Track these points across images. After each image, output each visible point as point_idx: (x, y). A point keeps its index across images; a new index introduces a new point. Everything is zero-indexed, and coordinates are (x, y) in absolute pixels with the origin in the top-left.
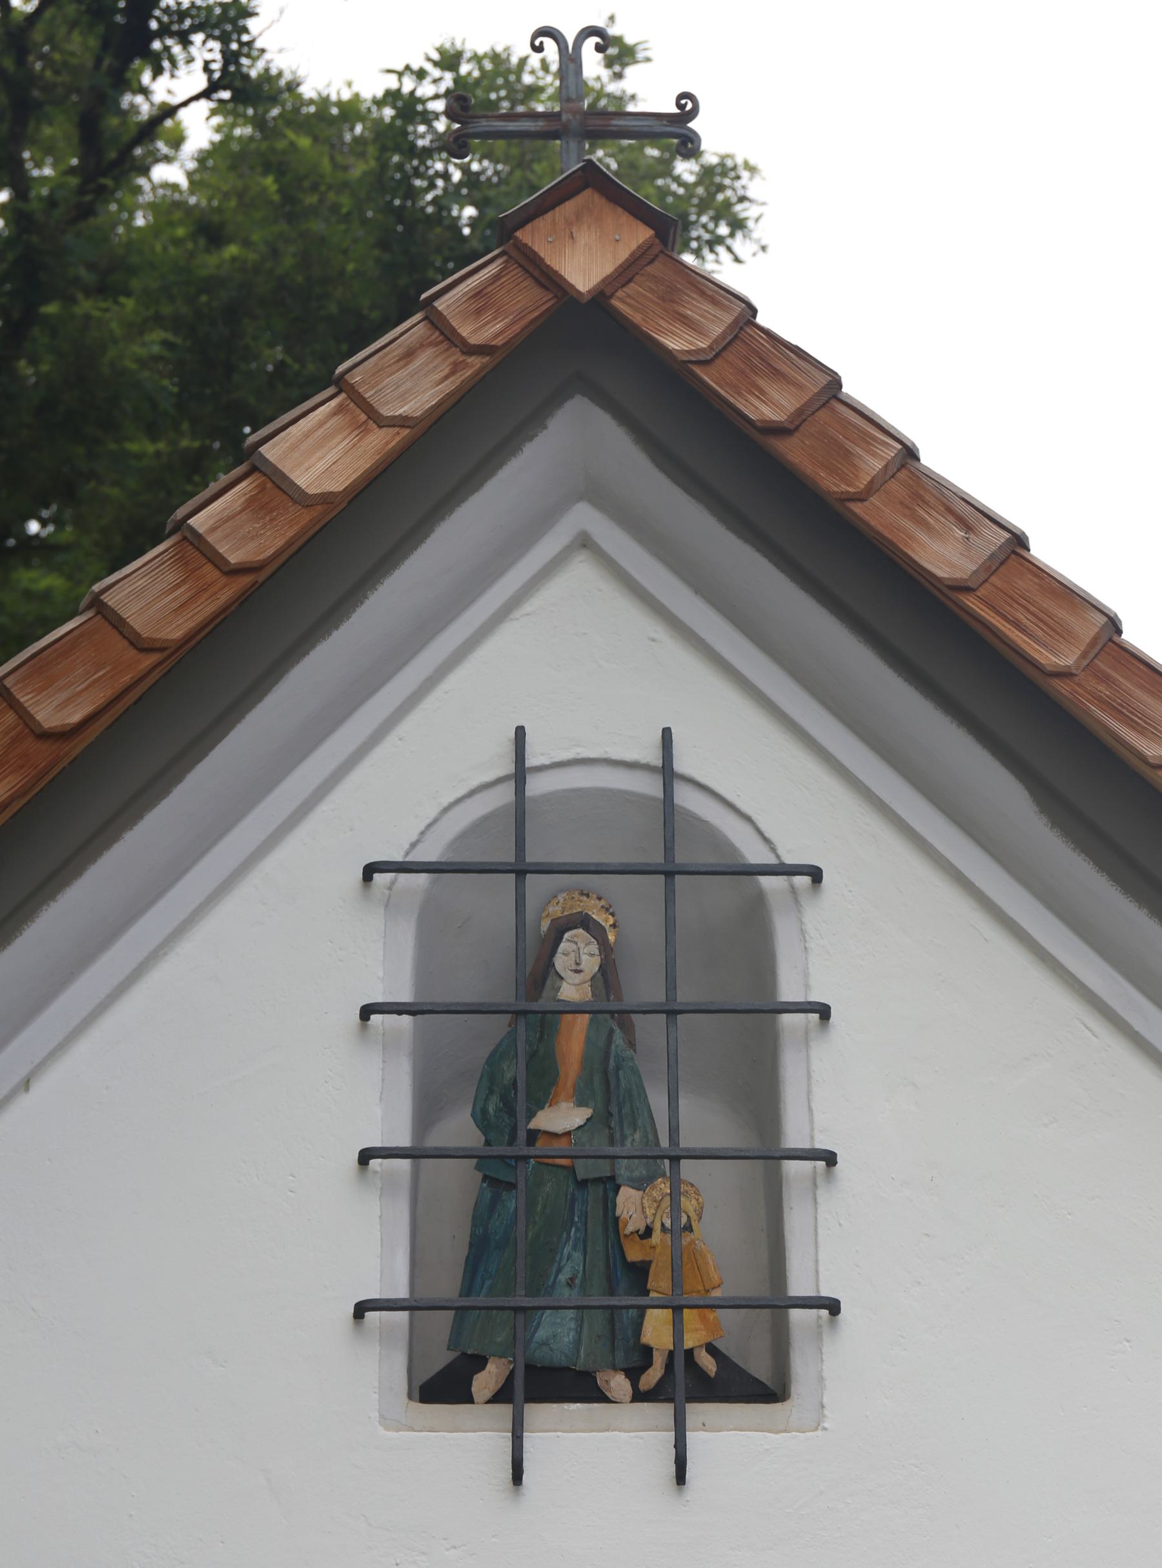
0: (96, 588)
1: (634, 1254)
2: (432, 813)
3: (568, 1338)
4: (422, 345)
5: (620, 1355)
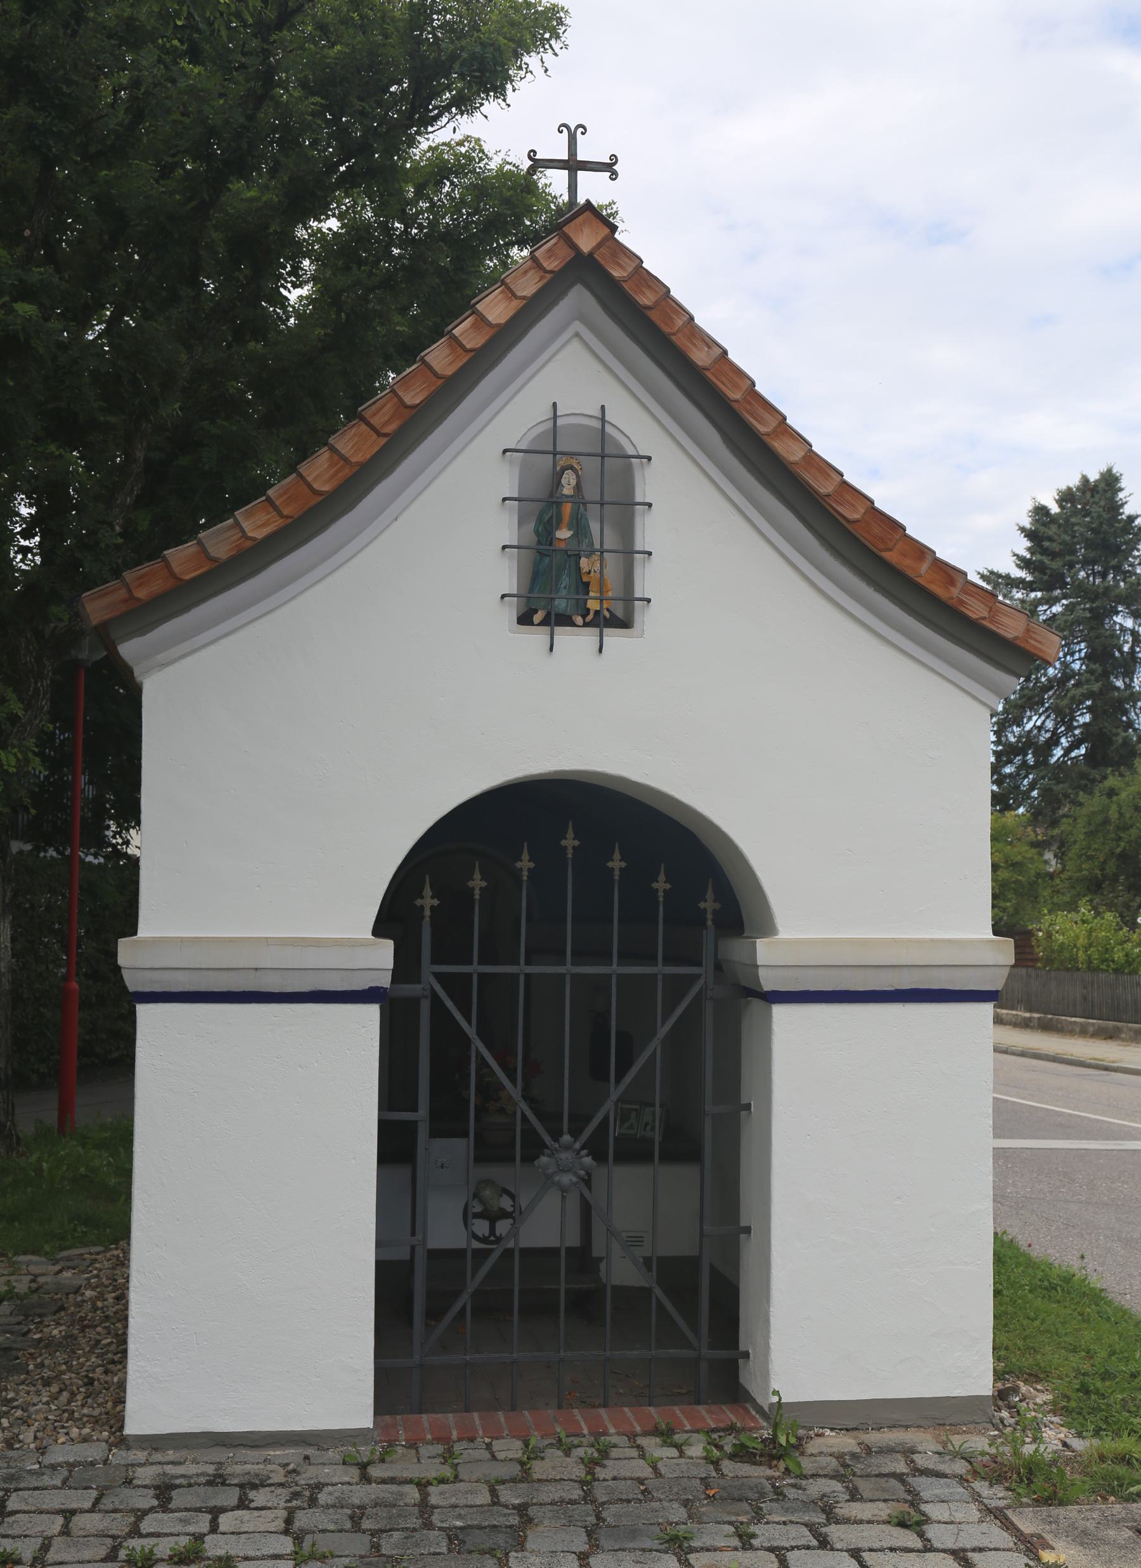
0: (422, 354)
1: (585, 579)
2: (525, 431)
3: (564, 605)
4: (530, 269)
5: (580, 611)
